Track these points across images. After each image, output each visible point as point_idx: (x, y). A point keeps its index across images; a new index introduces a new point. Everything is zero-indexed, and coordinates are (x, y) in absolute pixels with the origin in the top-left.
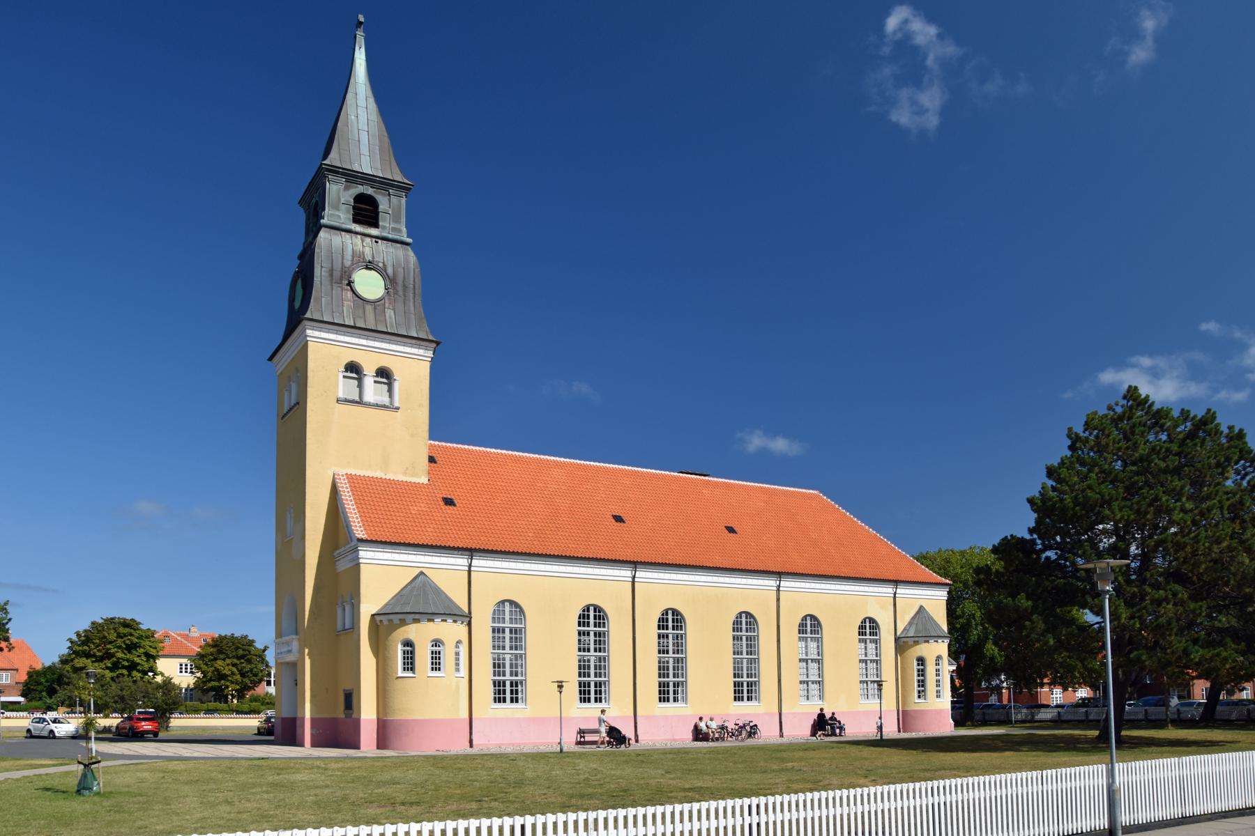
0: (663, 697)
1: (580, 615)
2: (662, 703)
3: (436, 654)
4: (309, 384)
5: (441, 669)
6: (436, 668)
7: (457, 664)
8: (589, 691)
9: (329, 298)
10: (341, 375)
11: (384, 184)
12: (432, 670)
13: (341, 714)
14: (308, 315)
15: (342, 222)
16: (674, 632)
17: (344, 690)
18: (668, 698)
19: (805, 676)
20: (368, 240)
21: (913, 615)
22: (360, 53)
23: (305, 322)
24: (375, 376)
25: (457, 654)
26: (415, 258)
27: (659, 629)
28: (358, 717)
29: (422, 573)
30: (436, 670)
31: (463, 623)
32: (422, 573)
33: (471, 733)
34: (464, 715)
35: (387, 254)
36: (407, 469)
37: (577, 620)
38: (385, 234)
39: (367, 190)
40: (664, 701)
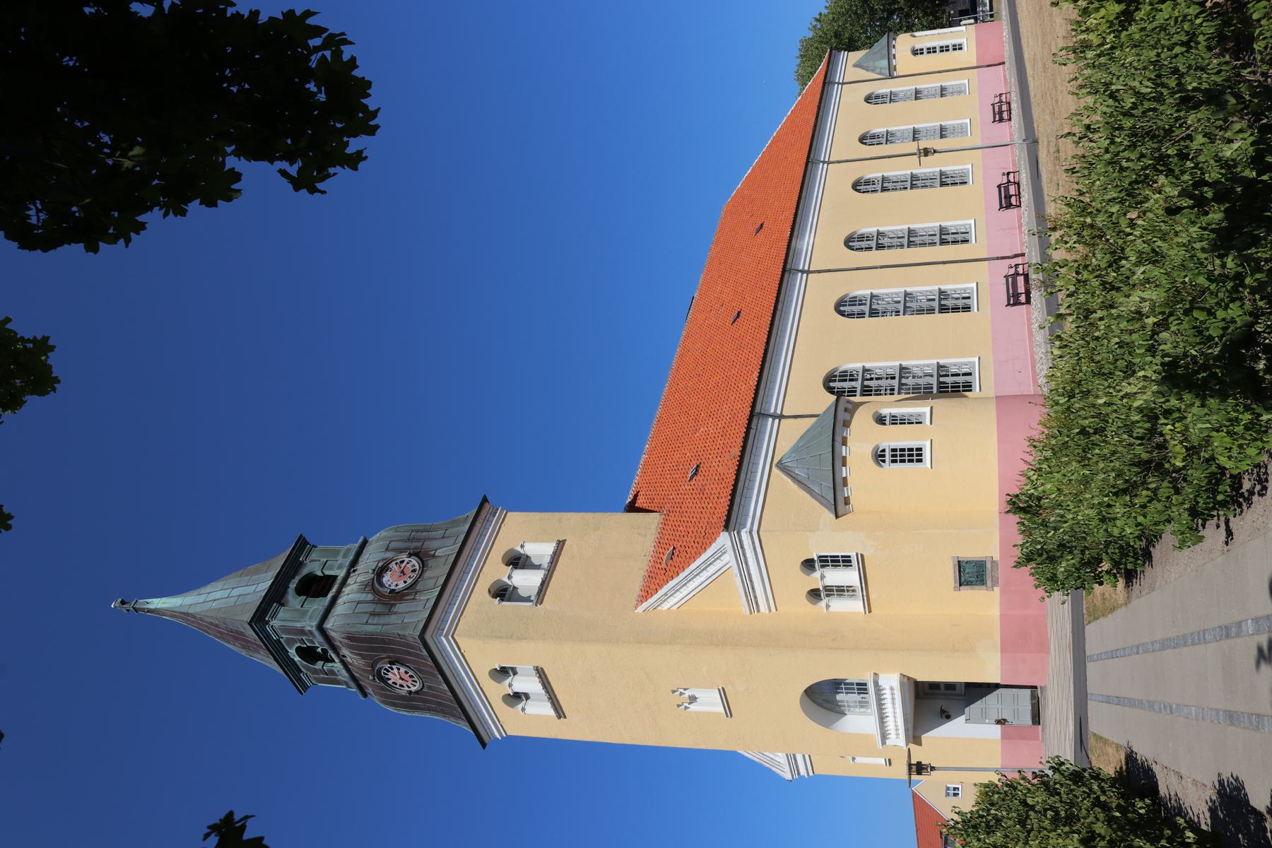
3: (896, 456)
5: (955, 51)
6: (917, 455)
11: (293, 564)
12: (920, 461)
20: (350, 581)
30: (921, 455)
35: (369, 561)
36: (639, 534)
39: (295, 582)
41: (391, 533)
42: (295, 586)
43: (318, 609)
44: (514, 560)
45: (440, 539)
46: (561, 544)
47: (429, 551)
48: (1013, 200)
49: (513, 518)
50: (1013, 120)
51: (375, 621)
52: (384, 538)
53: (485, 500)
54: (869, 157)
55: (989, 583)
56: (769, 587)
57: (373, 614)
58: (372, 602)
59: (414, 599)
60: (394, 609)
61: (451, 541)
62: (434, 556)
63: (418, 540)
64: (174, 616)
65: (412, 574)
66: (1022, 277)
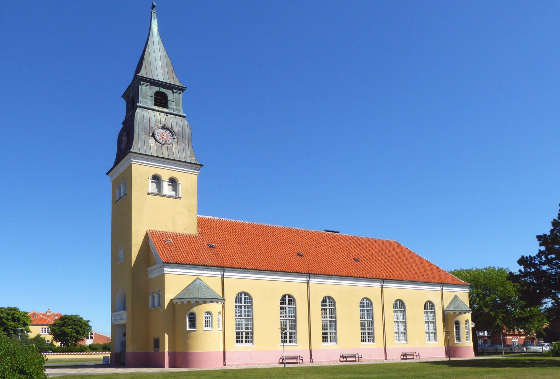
0: (325, 340)
1: (281, 299)
3: (208, 319)
4: (132, 185)
7: (219, 324)
10: (150, 181)
12: (206, 326)
13: (151, 349)
14: (132, 150)
15: (148, 105)
16: (329, 307)
17: (154, 338)
18: (327, 340)
19: (397, 330)
20: (163, 114)
22: (155, 21)
23: (130, 154)
24: (152, 179)
25: (219, 319)
27: (360, 307)
28: (163, 351)
29: (198, 278)
30: (208, 327)
31: (221, 303)
33: (224, 359)
34: (221, 350)
35: (173, 122)
36: (186, 227)
37: (234, 300)
50: (401, 360)
53: (202, 166)
55: (155, 349)
56: (239, 275)
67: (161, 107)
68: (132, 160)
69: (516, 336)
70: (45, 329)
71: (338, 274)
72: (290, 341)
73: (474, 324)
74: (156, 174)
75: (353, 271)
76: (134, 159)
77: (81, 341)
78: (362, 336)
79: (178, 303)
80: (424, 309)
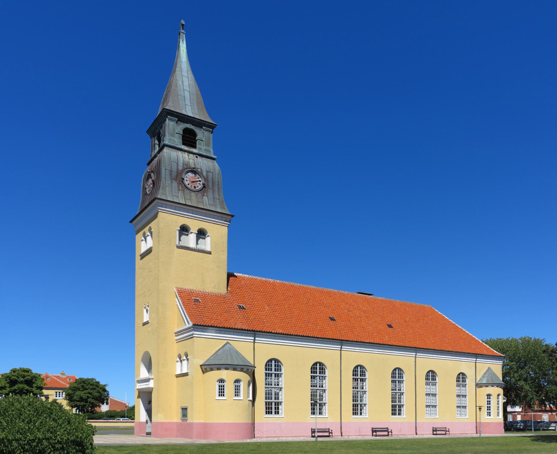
0: (269, 411)
2: (268, 414)
6: (222, 395)
8: (271, 408)
9: (170, 188)
11: (200, 124)
12: (219, 395)
15: (176, 144)
18: (357, 413)
19: (435, 403)
20: (191, 155)
21: (484, 372)
26: (218, 167)
30: (222, 396)
32: (228, 343)
35: (203, 164)
36: (215, 285)
38: (201, 153)
40: (355, 414)
41: (217, 172)
42: (189, 127)
43: (175, 142)
44: (203, 232)
45: (213, 197)
46: (210, 253)
47: (206, 193)
48: (375, 433)
49: (223, 230)
51: (167, 173)
52: (214, 169)
54: (342, 379)
55: (182, 419)
57: (171, 171)
58: (178, 170)
59: (179, 190)
60: (174, 182)
61: (212, 202)
62: (204, 195)
63: (213, 186)
64: (176, 63)
65: (193, 187)
66: (328, 435)
67: (189, 147)
68: (158, 207)
69: (547, 413)
70: (59, 393)
71: (371, 341)
72: (275, 412)
73: (506, 398)
74: (184, 224)
75: (386, 340)
76: (162, 207)
77: (98, 407)
78: (392, 409)
79: (207, 370)
80: (426, 380)
